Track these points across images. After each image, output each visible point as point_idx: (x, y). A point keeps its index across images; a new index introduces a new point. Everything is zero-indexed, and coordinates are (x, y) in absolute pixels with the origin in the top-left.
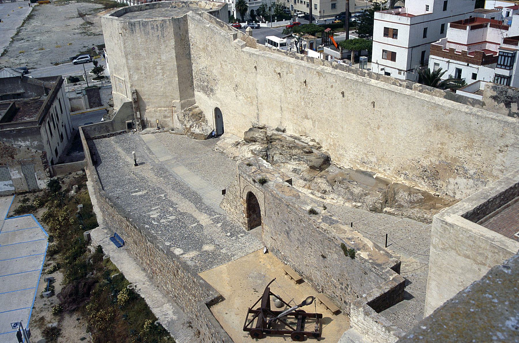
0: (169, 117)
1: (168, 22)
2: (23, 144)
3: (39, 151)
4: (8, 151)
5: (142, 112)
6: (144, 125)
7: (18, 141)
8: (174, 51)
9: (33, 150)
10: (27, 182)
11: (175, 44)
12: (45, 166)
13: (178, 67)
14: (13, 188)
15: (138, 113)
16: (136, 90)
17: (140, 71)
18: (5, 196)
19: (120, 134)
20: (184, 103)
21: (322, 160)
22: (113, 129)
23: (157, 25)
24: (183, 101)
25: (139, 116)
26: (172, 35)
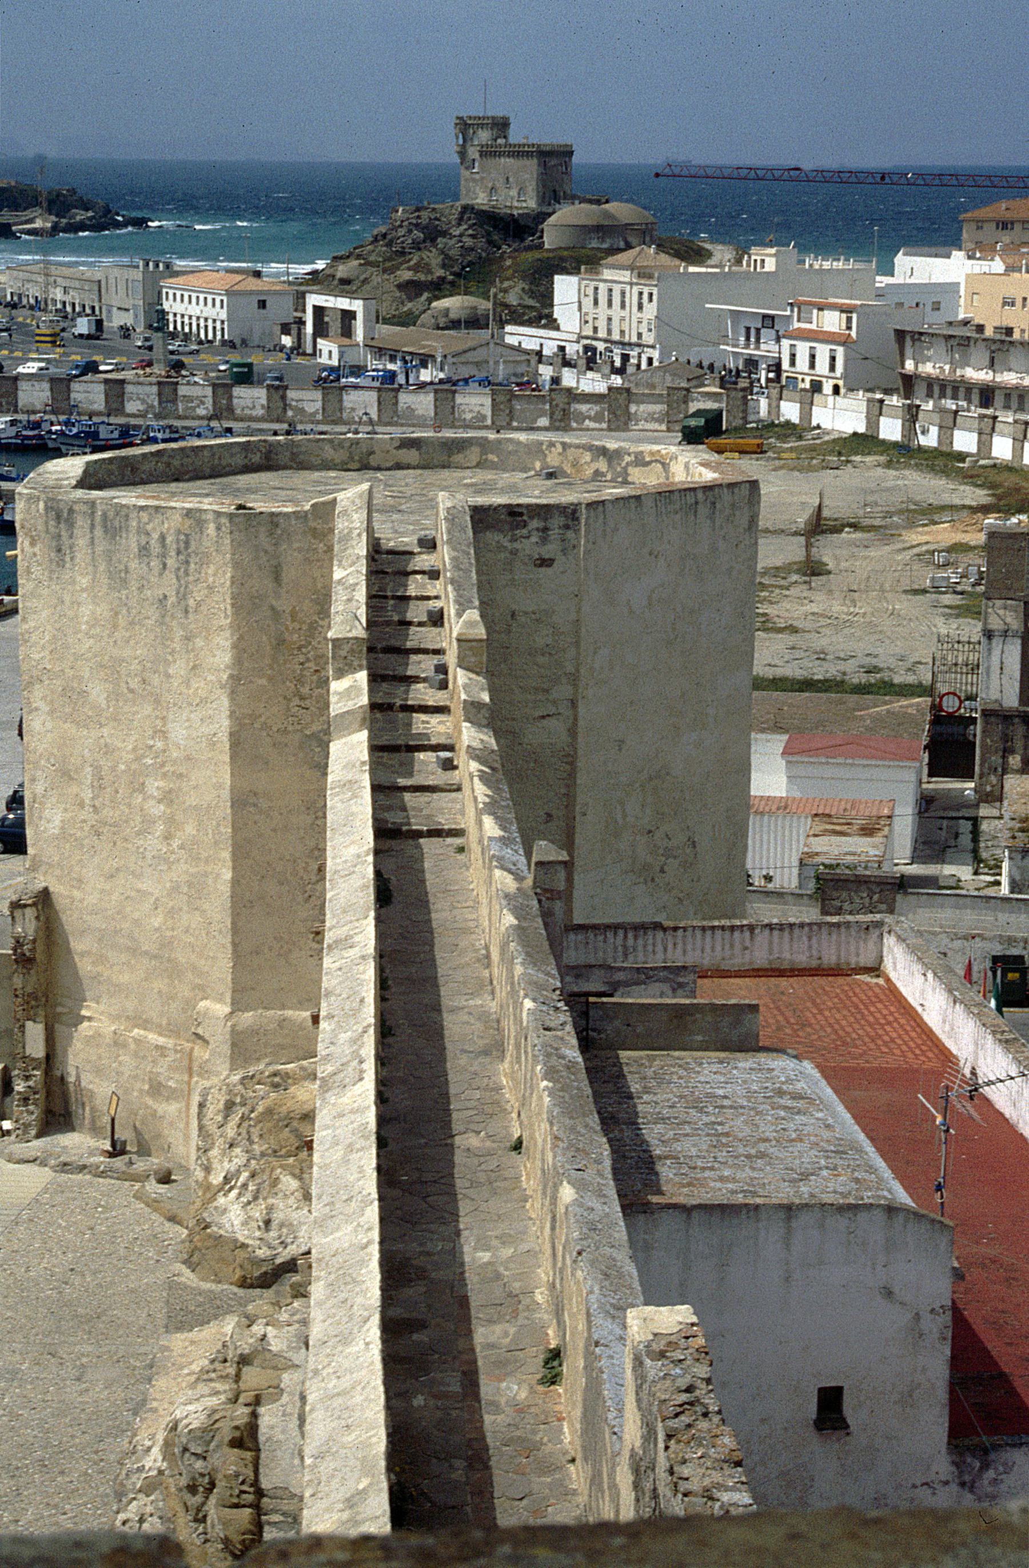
0: (172, 1095)
1: (212, 527)
6: (57, 1113)
8: (225, 702)
11: (238, 661)
13: (242, 802)
16: (46, 889)
17: (74, 789)
20: (254, 1032)
23: (163, 538)
24: (247, 1018)
25: (35, 1045)
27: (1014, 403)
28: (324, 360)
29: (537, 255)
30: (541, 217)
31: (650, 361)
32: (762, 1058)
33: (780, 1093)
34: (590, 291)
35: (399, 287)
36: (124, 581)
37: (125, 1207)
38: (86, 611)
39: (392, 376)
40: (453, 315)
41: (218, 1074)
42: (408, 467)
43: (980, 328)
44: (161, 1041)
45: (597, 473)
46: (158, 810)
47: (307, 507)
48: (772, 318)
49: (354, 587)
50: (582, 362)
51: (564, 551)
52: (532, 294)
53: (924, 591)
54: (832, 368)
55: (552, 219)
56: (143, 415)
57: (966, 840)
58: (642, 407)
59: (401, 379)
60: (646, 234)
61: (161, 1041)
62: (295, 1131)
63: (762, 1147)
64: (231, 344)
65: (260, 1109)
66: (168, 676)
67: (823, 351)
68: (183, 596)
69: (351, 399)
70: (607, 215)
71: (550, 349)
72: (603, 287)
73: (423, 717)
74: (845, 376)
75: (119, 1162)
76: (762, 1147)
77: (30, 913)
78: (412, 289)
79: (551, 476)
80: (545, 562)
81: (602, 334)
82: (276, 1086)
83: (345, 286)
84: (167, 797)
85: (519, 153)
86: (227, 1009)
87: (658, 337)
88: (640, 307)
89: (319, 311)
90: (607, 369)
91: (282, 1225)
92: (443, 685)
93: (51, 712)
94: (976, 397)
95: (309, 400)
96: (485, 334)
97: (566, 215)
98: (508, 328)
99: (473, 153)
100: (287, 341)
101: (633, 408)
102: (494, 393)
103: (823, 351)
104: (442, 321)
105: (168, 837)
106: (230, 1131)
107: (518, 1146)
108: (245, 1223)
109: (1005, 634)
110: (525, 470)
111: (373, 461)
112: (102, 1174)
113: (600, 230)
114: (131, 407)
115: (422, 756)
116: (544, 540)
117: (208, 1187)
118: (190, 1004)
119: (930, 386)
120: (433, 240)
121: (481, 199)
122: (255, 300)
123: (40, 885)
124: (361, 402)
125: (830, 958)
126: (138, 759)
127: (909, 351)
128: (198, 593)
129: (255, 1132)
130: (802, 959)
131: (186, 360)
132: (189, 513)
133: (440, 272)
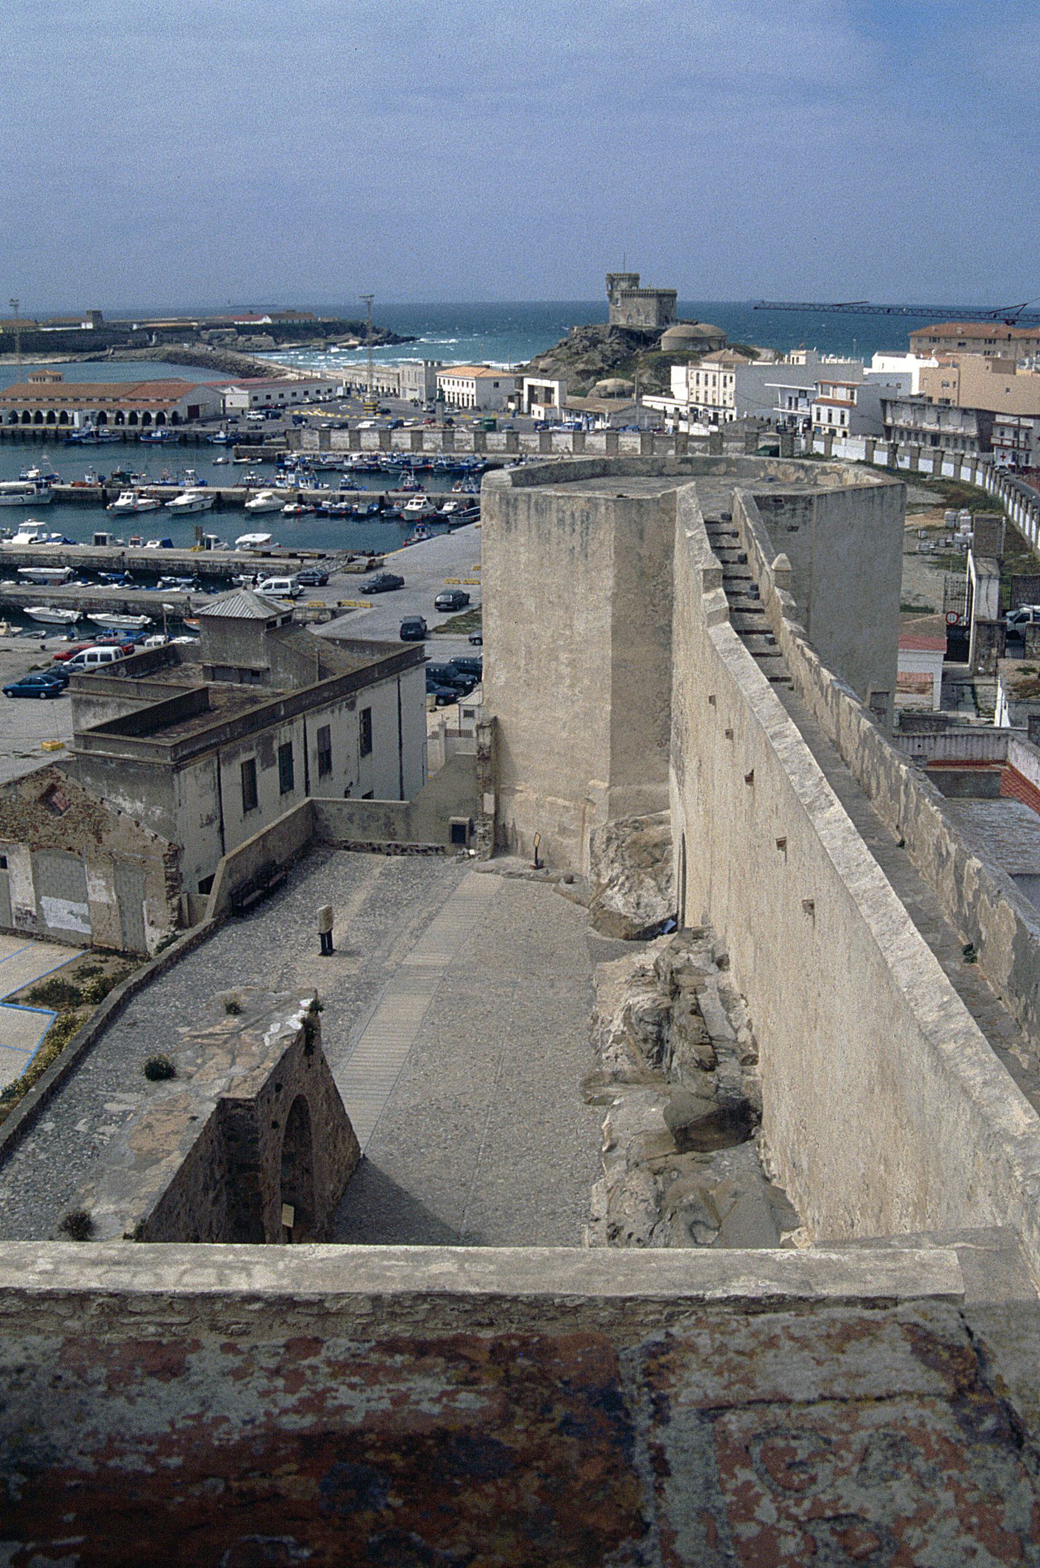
0: (574, 834)
1: (603, 509)
2: (127, 805)
3: (161, 839)
4: (90, 816)
5: (504, 798)
6: (502, 843)
7: (117, 793)
8: (609, 608)
9: (149, 833)
10: (123, 923)
11: (618, 584)
12: (172, 887)
13: (618, 665)
14: (86, 930)
15: (489, 799)
16: (495, 719)
18: (60, 943)
19: (425, 852)
21: (712, 1107)
22: (409, 832)
23: (573, 514)
24: (618, 790)
25: (489, 808)
26: (608, 554)
27: (952, 444)
28: (535, 417)
29: (658, 354)
30: (661, 332)
31: (731, 417)
32: (1003, 802)
33: (1021, 820)
34: (694, 376)
35: (578, 373)
36: (548, 541)
37: (550, 898)
38: (523, 558)
39: (579, 426)
40: (609, 390)
41: (600, 822)
42: (686, 474)
43: (930, 399)
44: (567, 803)
45: (798, 478)
46: (566, 670)
47: (659, 495)
48: (805, 392)
49: (702, 540)
50: (691, 418)
51: (804, 523)
52: (656, 377)
53: (915, 554)
54: (842, 422)
55: (666, 334)
56: (434, 451)
57: (969, 697)
58: (731, 444)
59: (584, 428)
60: (722, 343)
61: (567, 803)
62: (650, 854)
63: (1024, 847)
64: (478, 409)
65: (629, 840)
66: (575, 594)
67: (836, 412)
68: (584, 547)
69: (556, 439)
70: (698, 331)
71: (670, 410)
72: (702, 374)
73: (748, 615)
74: (850, 426)
75: (540, 872)
76: (1024, 847)
77: (487, 731)
78: (585, 374)
79: (771, 480)
80: (794, 529)
81: (702, 401)
82: (636, 828)
83: (544, 373)
84: (572, 664)
85: (645, 294)
86: (607, 785)
87: (736, 402)
88: (725, 385)
89: (531, 388)
90: (706, 422)
91: (646, 906)
92: (757, 597)
93: (501, 615)
94: (929, 440)
95: (533, 441)
96: (627, 402)
97: (673, 331)
98: (645, 397)
99: (617, 295)
100: (512, 406)
101: (725, 445)
102: (642, 436)
103: (836, 412)
104: (603, 394)
105: (572, 686)
106: (612, 855)
107: (902, 844)
108: (625, 905)
109: (989, 577)
110: (755, 477)
111: (665, 471)
112: (532, 879)
113: (695, 340)
114: (426, 446)
115: (755, 636)
116: (793, 516)
117: (599, 885)
118: (584, 782)
119: (902, 433)
120: (595, 346)
121: (622, 322)
122: (492, 382)
123: (492, 716)
124: (563, 441)
125: (977, 755)
126: (554, 641)
127: (889, 412)
128: (593, 546)
129: (626, 854)
130: (962, 756)
131: (455, 418)
132: (589, 499)
133: (601, 365)
